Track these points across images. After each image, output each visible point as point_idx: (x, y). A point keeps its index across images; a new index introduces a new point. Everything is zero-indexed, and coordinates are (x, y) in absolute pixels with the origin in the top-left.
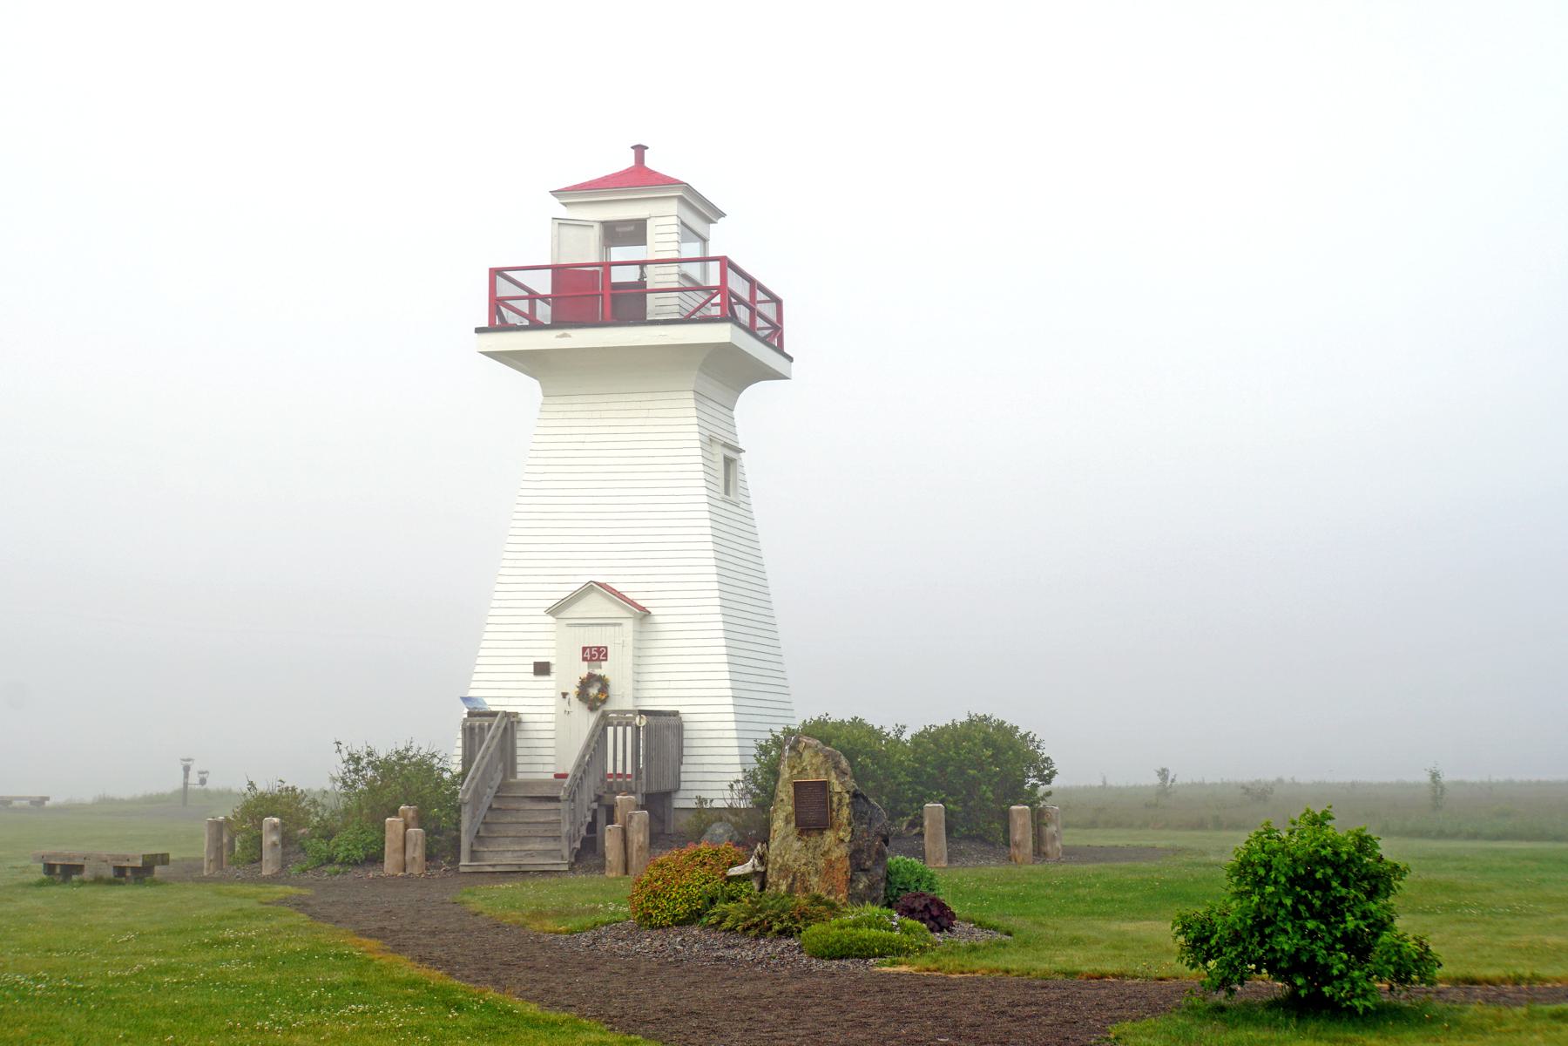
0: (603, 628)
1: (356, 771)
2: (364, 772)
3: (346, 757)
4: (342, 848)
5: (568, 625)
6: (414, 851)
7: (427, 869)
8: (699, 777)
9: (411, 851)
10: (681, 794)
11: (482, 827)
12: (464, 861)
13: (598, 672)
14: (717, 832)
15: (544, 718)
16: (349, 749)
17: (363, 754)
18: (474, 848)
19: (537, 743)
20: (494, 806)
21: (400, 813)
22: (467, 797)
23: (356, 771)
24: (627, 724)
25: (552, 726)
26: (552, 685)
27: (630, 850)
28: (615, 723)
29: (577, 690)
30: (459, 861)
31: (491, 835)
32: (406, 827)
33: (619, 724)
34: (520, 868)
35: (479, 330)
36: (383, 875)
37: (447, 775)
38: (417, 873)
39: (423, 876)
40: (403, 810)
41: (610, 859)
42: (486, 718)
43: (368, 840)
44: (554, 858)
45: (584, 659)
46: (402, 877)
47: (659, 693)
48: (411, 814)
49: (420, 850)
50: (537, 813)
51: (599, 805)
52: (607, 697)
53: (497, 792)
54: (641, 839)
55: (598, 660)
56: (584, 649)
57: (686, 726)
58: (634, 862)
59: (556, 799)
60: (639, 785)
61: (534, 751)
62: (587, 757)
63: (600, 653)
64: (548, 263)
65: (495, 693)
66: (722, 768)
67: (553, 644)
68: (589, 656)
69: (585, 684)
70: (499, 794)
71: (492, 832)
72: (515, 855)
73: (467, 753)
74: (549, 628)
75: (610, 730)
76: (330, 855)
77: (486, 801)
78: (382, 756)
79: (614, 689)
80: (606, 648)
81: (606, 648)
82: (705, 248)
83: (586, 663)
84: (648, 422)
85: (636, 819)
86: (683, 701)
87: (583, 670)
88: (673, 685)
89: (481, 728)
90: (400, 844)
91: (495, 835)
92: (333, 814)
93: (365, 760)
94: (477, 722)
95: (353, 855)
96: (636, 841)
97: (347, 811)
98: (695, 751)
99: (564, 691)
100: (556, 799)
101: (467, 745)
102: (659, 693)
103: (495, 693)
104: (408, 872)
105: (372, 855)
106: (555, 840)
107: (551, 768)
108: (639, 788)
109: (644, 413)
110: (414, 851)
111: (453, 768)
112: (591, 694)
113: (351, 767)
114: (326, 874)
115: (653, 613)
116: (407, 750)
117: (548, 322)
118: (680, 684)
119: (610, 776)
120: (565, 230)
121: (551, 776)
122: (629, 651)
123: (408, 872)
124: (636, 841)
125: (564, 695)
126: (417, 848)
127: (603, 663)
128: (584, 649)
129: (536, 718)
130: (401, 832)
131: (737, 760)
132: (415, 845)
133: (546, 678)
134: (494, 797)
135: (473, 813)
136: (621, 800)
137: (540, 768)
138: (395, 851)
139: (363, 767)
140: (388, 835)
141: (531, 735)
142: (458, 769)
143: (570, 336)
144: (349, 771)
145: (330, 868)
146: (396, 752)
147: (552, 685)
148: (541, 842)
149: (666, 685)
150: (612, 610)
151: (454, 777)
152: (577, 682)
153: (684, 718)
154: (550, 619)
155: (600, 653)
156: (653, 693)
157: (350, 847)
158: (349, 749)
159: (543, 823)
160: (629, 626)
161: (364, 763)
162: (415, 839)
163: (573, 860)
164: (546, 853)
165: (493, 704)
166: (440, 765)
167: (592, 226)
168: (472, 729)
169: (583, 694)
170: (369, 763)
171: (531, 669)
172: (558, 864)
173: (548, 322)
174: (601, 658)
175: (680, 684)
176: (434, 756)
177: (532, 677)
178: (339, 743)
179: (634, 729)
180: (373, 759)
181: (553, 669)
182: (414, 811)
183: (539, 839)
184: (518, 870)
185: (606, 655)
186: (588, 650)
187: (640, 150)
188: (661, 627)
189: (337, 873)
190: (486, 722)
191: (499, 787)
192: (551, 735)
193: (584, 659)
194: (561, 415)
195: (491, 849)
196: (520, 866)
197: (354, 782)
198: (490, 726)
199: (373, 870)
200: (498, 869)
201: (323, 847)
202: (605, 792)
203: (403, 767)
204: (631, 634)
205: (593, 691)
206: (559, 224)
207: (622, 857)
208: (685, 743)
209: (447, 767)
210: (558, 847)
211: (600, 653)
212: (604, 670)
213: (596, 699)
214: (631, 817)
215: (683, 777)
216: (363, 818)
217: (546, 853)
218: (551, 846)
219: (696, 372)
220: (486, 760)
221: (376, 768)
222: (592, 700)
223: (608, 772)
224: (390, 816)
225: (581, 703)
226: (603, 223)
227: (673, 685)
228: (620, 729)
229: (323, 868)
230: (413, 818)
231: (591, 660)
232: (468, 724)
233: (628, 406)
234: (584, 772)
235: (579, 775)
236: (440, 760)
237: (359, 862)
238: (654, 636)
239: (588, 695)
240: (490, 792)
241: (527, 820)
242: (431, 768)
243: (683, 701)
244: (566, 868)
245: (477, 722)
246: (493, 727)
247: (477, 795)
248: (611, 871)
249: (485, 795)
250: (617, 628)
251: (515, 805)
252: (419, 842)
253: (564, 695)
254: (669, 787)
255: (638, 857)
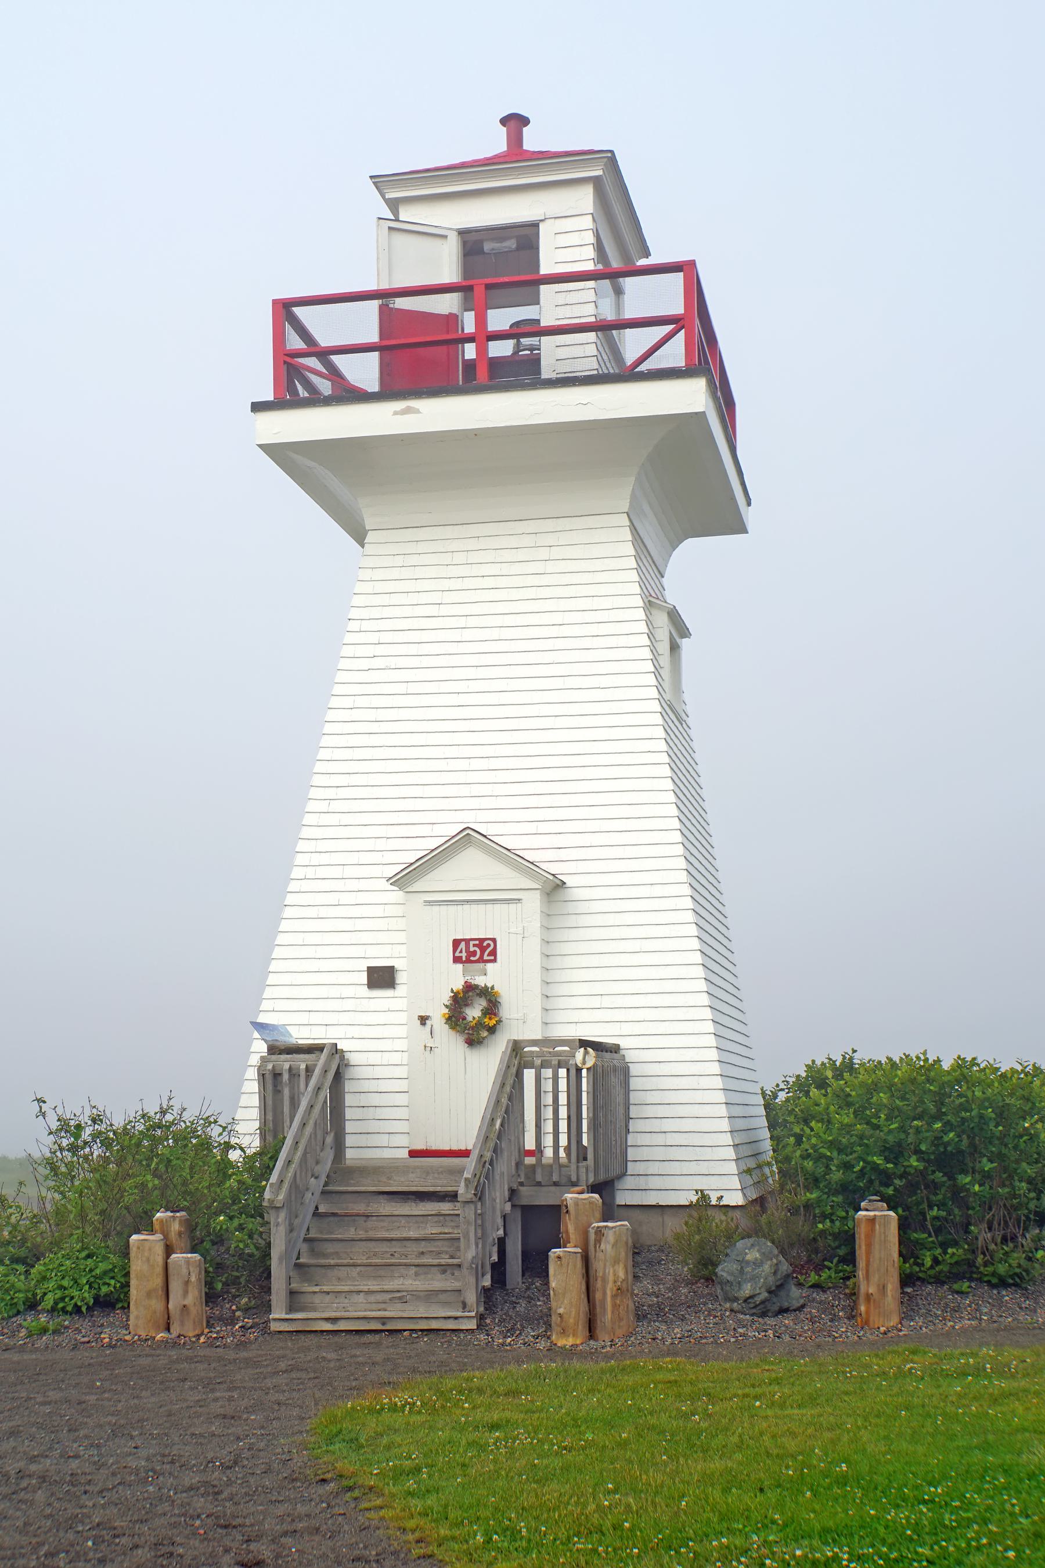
0: (489, 907)
1: (73, 1149)
2: (87, 1150)
3: (55, 1125)
4: (51, 1285)
5: (429, 903)
6: (186, 1293)
7: (209, 1325)
8: (659, 1153)
9: (180, 1292)
10: (629, 1182)
11: (304, 1247)
12: (278, 1312)
13: (480, 981)
14: (748, 1257)
15: (387, 1058)
16: (60, 1111)
17: (85, 1119)
18: (294, 1286)
19: (375, 1099)
20: (322, 1209)
21: (156, 1226)
22: (281, 1197)
23: (73, 1149)
24: (560, 1065)
25: (402, 1072)
26: (402, 1004)
27: (598, 1296)
28: (538, 1062)
29: (446, 1011)
30: (270, 1311)
31: (323, 1261)
32: (169, 1250)
33: (544, 1065)
34: (384, 1324)
35: (258, 407)
36: (127, 1338)
37: (234, 1155)
38: (191, 1334)
39: (202, 1340)
40: (161, 1221)
41: (561, 1311)
42: (302, 1056)
43: (98, 1271)
44: (446, 1304)
45: (457, 960)
46: (165, 1342)
47: (585, 1015)
48: (176, 1227)
49: (196, 1293)
50: (403, 1220)
51: (513, 1206)
52: (499, 1022)
53: (326, 1184)
54: (621, 1274)
55: (481, 960)
56: (456, 943)
57: (634, 1070)
58: (607, 1317)
59: (453, 1197)
60: (583, 1170)
61: (370, 1113)
62: (498, 1123)
63: (483, 951)
64: (372, 286)
65: (303, 1018)
66: (696, 1140)
67: (401, 937)
68: (464, 955)
69: (459, 1001)
70: (330, 1188)
71: (325, 1256)
72: (372, 1298)
73: (270, 1117)
74: (391, 910)
75: (529, 1075)
76: (30, 1295)
77: (310, 1200)
78: (118, 1122)
79: (508, 1010)
80: (494, 940)
81: (494, 940)
82: (619, 306)
83: (460, 966)
84: (550, 567)
85: (610, 1237)
86: (627, 1029)
87: (456, 978)
88: (607, 1002)
89: (293, 1073)
90: (159, 1281)
91: (332, 1262)
92: (36, 1220)
93: (88, 1131)
94: (285, 1062)
95: (72, 1298)
96: (611, 1278)
97: (60, 1214)
98: (650, 1111)
99: (423, 1014)
100: (453, 1197)
101: (270, 1102)
102: (585, 1015)
103: (303, 1018)
104: (175, 1332)
105: (106, 1295)
106: (444, 1272)
107: (403, 1141)
108: (583, 1177)
109: (543, 554)
110: (186, 1293)
111: (245, 1142)
112: (470, 1018)
113: (65, 1143)
114: (23, 1333)
115: (568, 884)
116: (163, 1112)
117: (374, 387)
118: (620, 1001)
119: (530, 1153)
120: (399, 239)
121: (404, 1154)
122: (534, 944)
123: (175, 1332)
124: (611, 1278)
125: (423, 1020)
126: (190, 1288)
127: (489, 966)
128: (456, 943)
129: (374, 1059)
130: (160, 1259)
131: (725, 1125)
132: (187, 1283)
133: (389, 993)
134: (323, 1193)
135: (291, 1224)
136: (577, 1203)
137: (383, 1140)
138: (149, 1294)
139: (86, 1143)
140: (137, 1266)
141: (366, 1086)
142: (253, 1143)
143: (417, 411)
144: (61, 1149)
145: (29, 1321)
146: (143, 1116)
147: (402, 1004)
148: (417, 1274)
149: (596, 1002)
150: (508, 878)
151: (249, 1160)
152: (446, 997)
153: (630, 1056)
154: (398, 895)
155: (483, 950)
156: (574, 1016)
157: (65, 1283)
158: (60, 1111)
159: (417, 1240)
160: (533, 902)
161: (86, 1134)
162: (184, 1271)
163: (482, 1309)
164: (430, 1296)
165: (301, 1036)
166: (222, 1139)
167: (445, 237)
168: (277, 1075)
169: (455, 1018)
170: (95, 1136)
171: (364, 978)
172: (456, 1318)
173: (374, 387)
174: (486, 957)
175: (620, 1001)
176: (208, 1122)
177: (364, 991)
178: (41, 1101)
179: (573, 1072)
180: (102, 1128)
181: (400, 978)
182: (180, 1221)
183: (413, 1269)
184: (380, 1327)
185: (494, 953)
186: (463, 945)
187: (515, 122)
188: (582, 907)
189: (44, 1331)
190: (301, 1062)
191: (328, 1177)
192: (403, 1086)
193: (457, 960)
194: (399, 561)
195: (326, 1288)
196: (383, 1320)
197: (70, 1166)
198: (309, 1070)
199: (111, 1325)
200: (342, 1326)
201: (19, 1282)
202: (521, 1184)
203: (155, 1141)
204: (538, 916)
205: (473, 1013)
206: (390, 228)
207: (584, 1307)
208: (634, 1098)
209: (237, 1141)
210: (457, 1285)
211: (483, 950)
212: (490, 976)
213: (479, 1025)
214: (599, 1232)
215: (631, 1154)
216: (89, 1229)
217: (430, 1296)
218: (438, 1282)
219: (632, 480)
220: (309, 1129)
221: (107, 1144)
222: (473, 1028)
223: (527, 1148)
224: (138, 1231)
225: (452, 1033)
226: (462, 233)
227: (607, 1002)
228: (548, 1073)
229: (19, 1319)
230: (180, 1234)
231: (468, 961)
232: (270, 1066)
233: (513, 542)
234: (495, 1151)
235: (488, 1155)
236: (224, 1128)
237: (84, 1309)
238: (572, 921)
239: (464, 1019)
240: (316, 1185)
241: (387, 1235)
242: (206, 1144)
243: (627, 1029)
244: (472, 1325)
245: (285, 1062)
246: (317, 1071)
247: (297, 1191)
248: (564, 1332)
249: (307, 1189)
250: (513, 906)
251: (360, 1208)
252: (193, 1279)
253: (423, 1020)
254: (612, 1174)
255: (615, 1306)
